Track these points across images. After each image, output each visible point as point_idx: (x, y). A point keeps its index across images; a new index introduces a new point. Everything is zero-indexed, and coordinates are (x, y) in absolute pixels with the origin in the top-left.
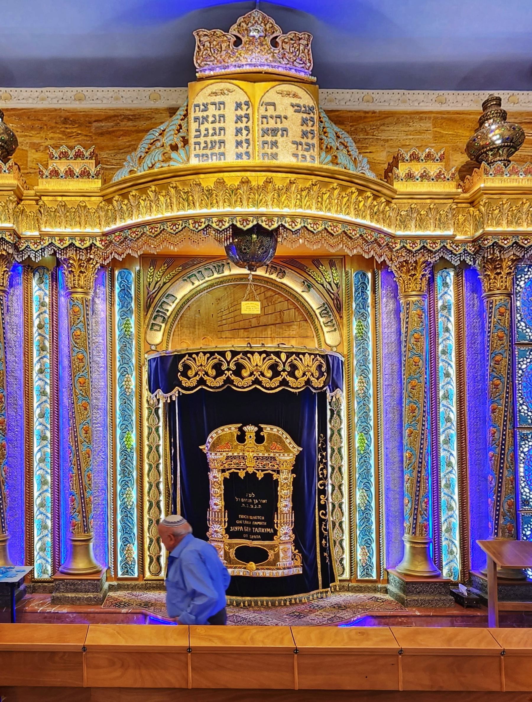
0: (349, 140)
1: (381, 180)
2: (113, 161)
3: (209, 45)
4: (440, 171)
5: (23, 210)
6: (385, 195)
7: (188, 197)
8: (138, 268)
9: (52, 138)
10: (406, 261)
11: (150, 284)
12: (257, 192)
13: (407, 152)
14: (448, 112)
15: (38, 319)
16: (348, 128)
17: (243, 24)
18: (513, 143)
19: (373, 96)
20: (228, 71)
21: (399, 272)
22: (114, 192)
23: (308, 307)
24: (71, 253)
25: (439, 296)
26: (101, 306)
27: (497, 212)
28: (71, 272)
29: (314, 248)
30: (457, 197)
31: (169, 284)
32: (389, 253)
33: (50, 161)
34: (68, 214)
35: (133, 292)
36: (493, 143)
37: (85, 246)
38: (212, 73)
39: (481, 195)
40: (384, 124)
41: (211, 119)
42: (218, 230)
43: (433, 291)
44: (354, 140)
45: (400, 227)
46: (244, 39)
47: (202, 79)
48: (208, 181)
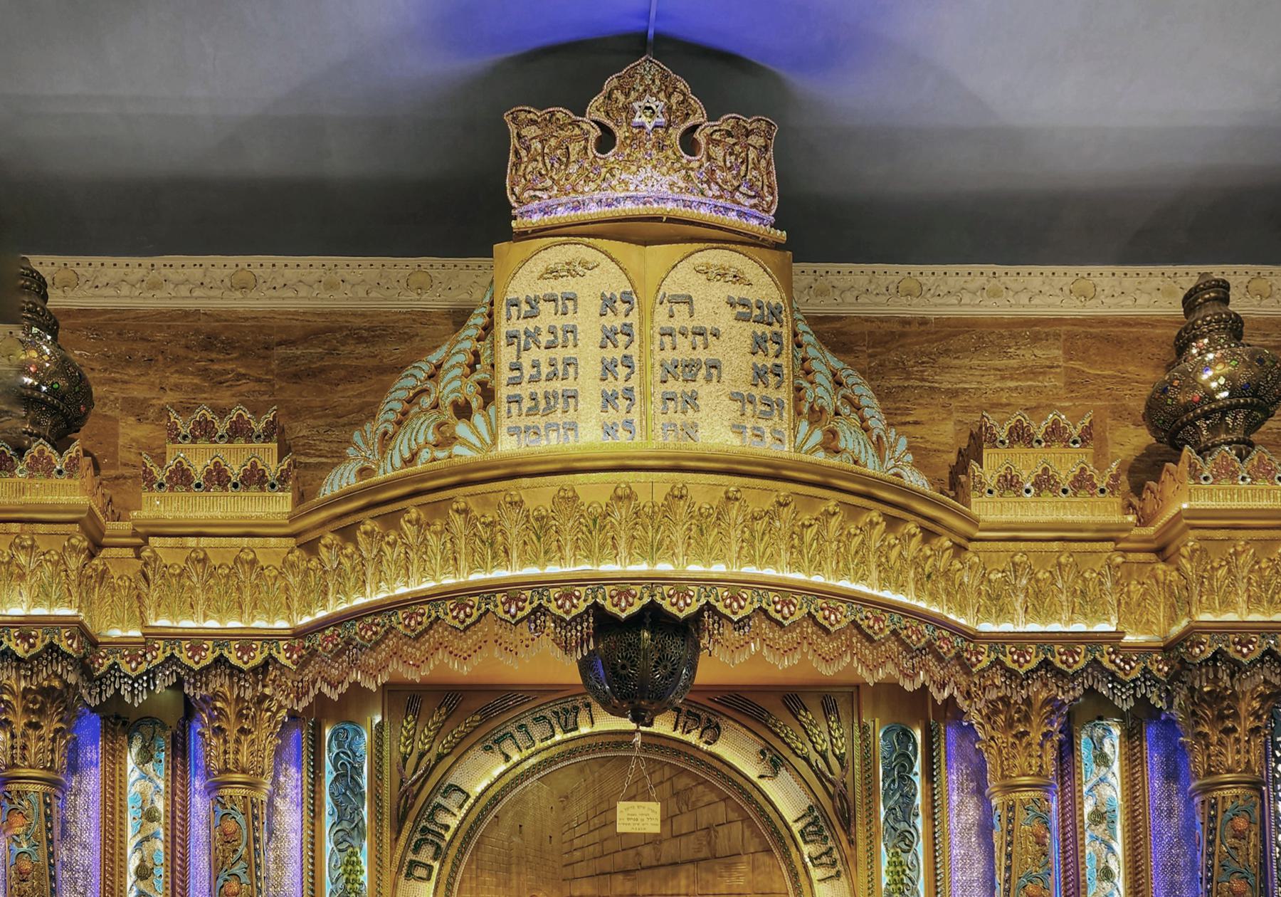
0: (864, 392)
1: (942, 492)
2: (324, 446)
3: (539, 146)
4: (1083, 470)
5: (105, 572)
6: (950, 529)
7: (493, 535)
8: (378, 719)
10: (1003, 699)
11: (405, 760)
12: (649, 526)
13: (1001, 422)
14: (1102, 321)
15: (138, 855)
16: (864, 362)
17: (618, 94)
18: (1256, 400)
19: (922, 279)
20: (582, 214)
21: (988, 727)
22: (323, 524)
23: (773, 815)
24: (218, 683)
25: (1085, 789)
26: (290, 817)
27: (1222, 573)
28: (219, 731)
29: (782, 665)
30: (1124, 535)
31: (449, 761)
32: (962, 680)
33: (170, 446)
34: (212, 582)
35: (365, 782)
36: (1210, 395)
37: (252, 664)
38: (547, 220)
39: (1183, 531)
40: (947, 352)
41: (545, 338)
42: (563, 620)
43: (1072, 775)
44: (881, 395)
45: (989, 612)
46: (620, 134)
47: (524, 235)
48: (539, 495)
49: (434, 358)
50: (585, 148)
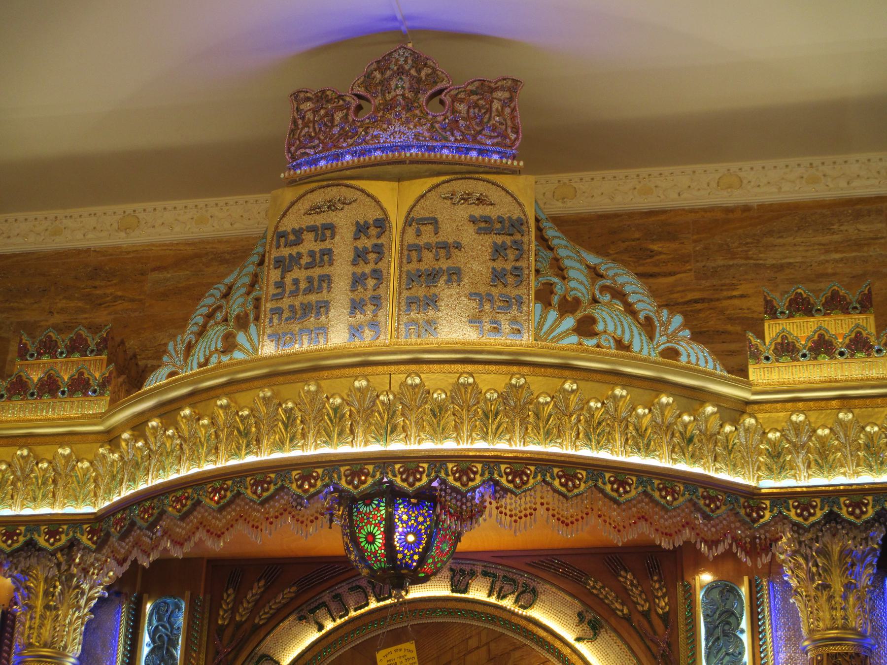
9: (62, 311)
40: (770, 233)
41: (305, 260)
49: (229, 280)
50: (347, 115)
